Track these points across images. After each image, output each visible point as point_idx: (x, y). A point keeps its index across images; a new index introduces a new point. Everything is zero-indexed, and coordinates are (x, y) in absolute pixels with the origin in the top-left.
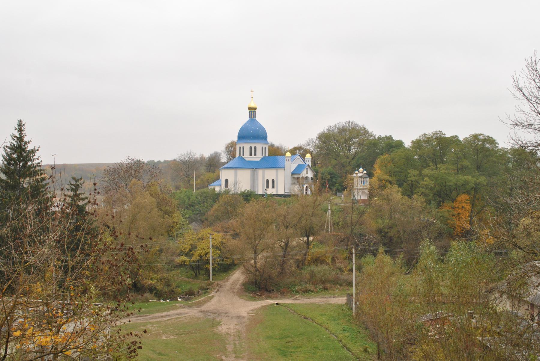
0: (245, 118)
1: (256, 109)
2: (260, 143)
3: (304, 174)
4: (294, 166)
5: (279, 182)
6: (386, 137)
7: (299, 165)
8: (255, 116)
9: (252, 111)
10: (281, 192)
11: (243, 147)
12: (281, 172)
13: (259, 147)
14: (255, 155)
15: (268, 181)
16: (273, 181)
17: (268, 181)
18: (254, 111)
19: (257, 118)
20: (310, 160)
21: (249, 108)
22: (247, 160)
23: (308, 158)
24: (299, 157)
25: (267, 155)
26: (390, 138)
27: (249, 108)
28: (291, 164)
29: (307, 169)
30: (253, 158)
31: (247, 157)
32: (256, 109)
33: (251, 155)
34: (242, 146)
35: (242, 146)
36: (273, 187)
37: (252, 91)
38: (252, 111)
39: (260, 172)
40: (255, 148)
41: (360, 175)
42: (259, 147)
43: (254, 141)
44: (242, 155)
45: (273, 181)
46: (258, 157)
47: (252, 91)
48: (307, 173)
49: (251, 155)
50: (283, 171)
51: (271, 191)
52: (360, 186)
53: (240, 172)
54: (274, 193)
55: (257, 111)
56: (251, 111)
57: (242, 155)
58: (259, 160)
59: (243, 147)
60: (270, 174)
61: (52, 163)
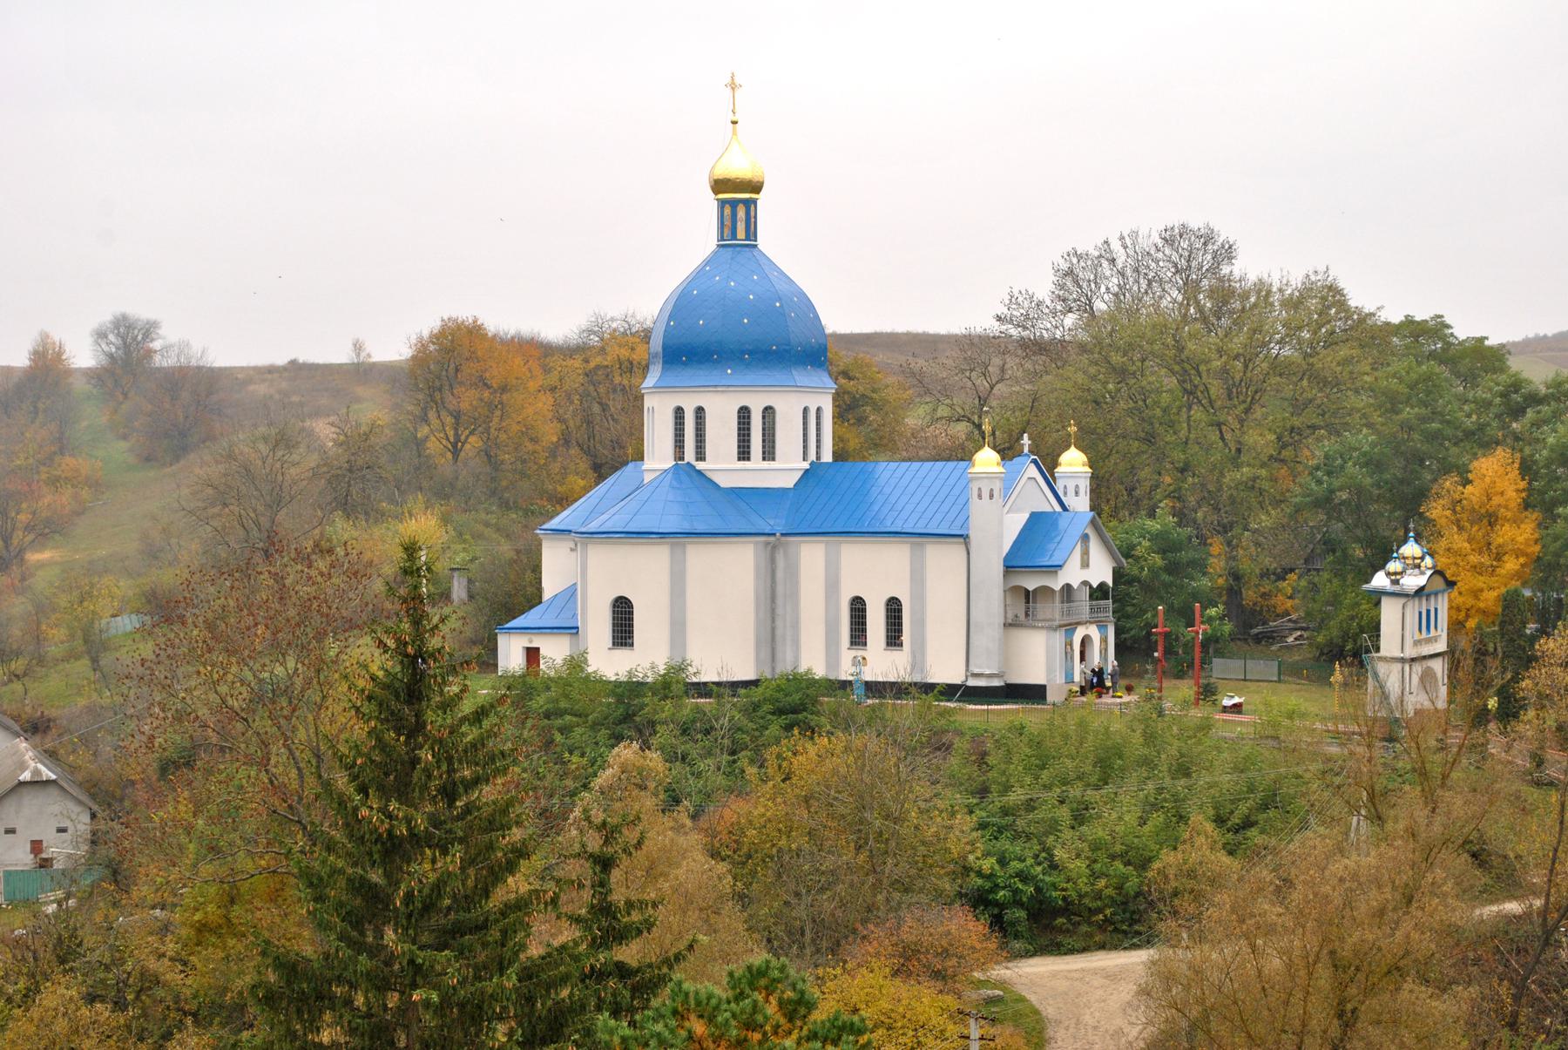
1: (756, 187)
4: (1015, 523)
6: (1409, 321)
7: (1036, 519)
8: (751, 233)
9: (737, 200)
10: (946, 669)
11: (700, 412)
12: (943, 562)
13: (789, 408)
14: (769, 453)
15: (858, 608)
16: (894, 609)
17: (858, 608)
19: (764, 241)
20: (1085, 485)
21: (719, 186)
22: (724, 481)
23: (1073, 476)
25: (827, 457)
26: (1436, 329)
27: (719, 186)
29: (1085, 538)
30: (758, 474)
31: (722, 464)
32: (756, 187)
33: (744, 454)
35: (689, 404)
36: (894, 638)
37: (733, 86)
38: (737, 200)
39: (811, 556)
40: (769, 412)
41: (1412, 581)
42: (789, 408)
43: (777, 376)
45: (894, 609)
46: (786, 469)
47: (733, 86)
48: (1085, 564)
49: (744, 454)
50: (955, 552)
51: (882, 664)
52: (1417, 643)
53: (703, 559)
55: (762, 198)
56: (734, 204)
58: (789, 481)
59: (700, 412)
60: (874, 571)
61: (716, 679)
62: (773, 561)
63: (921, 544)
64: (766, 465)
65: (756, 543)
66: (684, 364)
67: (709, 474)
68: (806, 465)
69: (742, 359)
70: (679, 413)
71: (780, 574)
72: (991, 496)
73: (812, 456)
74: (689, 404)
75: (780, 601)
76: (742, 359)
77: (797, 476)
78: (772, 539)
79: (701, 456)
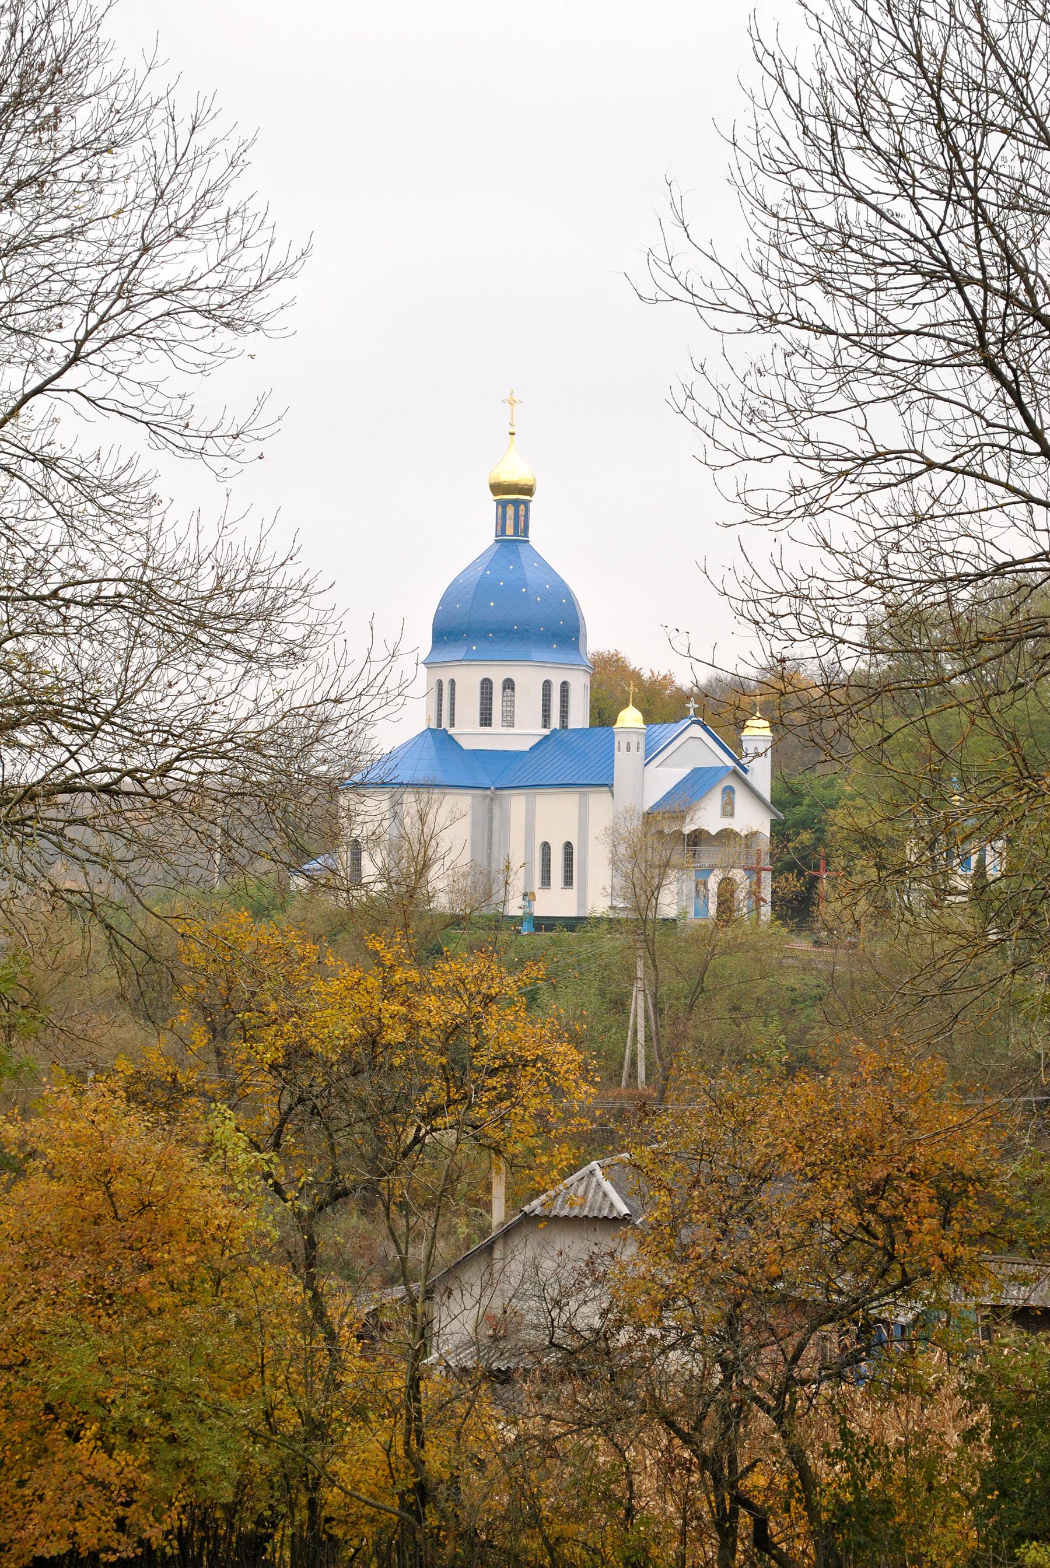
0: (477, 533)
1: (528, 490)
2: (470, 659)
3: (709, 818)
4: (662, 779)
5: (564, 857)
7: (696, 771)
8: (522, 527)
9: (513, 499)
10: (599, 905)
11: (453, 682)
12: (599, 804)
13: (529, 679)
14: (509, 721)
15: (546, 846)
16: (568, 846)
18: (516, 503)
21: (497, 488)
22: (467, 744)
23: (630, 730)
24: (697, 731)
27: (497, 488)
28: (649, 771)
30: (499, 738)
31: (469, 733)
32: (528, 490)
34: (497, 675)
38: (513, 499)
39: (517, 803)
40: (565, 686)
44: (446, 724)
48: (728, 811)
51: (556, 903)
54: (572, 912)
55: (537, 505)
57: (446, 724)
62: (491, 812)
63: (585, 793)
64: (504, 730)
65: (474, 795)
66: (445, 642)
67: (456, 738)
68: (546, 732)
69: (487, 638)
70: (547, 685)
71: (496, 824)
72: (628, 749)
73: (555, 722)
74: (497, 675)
75: (495, 848)
76: (487, 638)
77: (535, 741)
78: (489, 792)
79: (452, 725)
